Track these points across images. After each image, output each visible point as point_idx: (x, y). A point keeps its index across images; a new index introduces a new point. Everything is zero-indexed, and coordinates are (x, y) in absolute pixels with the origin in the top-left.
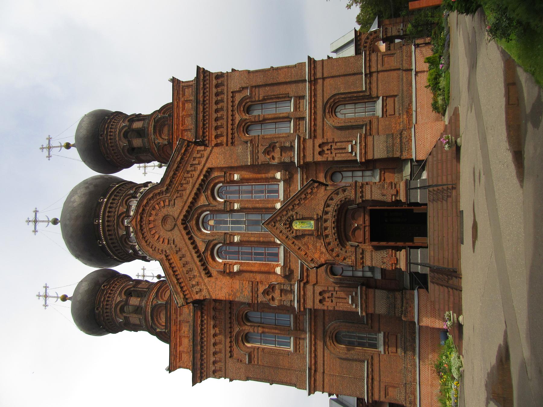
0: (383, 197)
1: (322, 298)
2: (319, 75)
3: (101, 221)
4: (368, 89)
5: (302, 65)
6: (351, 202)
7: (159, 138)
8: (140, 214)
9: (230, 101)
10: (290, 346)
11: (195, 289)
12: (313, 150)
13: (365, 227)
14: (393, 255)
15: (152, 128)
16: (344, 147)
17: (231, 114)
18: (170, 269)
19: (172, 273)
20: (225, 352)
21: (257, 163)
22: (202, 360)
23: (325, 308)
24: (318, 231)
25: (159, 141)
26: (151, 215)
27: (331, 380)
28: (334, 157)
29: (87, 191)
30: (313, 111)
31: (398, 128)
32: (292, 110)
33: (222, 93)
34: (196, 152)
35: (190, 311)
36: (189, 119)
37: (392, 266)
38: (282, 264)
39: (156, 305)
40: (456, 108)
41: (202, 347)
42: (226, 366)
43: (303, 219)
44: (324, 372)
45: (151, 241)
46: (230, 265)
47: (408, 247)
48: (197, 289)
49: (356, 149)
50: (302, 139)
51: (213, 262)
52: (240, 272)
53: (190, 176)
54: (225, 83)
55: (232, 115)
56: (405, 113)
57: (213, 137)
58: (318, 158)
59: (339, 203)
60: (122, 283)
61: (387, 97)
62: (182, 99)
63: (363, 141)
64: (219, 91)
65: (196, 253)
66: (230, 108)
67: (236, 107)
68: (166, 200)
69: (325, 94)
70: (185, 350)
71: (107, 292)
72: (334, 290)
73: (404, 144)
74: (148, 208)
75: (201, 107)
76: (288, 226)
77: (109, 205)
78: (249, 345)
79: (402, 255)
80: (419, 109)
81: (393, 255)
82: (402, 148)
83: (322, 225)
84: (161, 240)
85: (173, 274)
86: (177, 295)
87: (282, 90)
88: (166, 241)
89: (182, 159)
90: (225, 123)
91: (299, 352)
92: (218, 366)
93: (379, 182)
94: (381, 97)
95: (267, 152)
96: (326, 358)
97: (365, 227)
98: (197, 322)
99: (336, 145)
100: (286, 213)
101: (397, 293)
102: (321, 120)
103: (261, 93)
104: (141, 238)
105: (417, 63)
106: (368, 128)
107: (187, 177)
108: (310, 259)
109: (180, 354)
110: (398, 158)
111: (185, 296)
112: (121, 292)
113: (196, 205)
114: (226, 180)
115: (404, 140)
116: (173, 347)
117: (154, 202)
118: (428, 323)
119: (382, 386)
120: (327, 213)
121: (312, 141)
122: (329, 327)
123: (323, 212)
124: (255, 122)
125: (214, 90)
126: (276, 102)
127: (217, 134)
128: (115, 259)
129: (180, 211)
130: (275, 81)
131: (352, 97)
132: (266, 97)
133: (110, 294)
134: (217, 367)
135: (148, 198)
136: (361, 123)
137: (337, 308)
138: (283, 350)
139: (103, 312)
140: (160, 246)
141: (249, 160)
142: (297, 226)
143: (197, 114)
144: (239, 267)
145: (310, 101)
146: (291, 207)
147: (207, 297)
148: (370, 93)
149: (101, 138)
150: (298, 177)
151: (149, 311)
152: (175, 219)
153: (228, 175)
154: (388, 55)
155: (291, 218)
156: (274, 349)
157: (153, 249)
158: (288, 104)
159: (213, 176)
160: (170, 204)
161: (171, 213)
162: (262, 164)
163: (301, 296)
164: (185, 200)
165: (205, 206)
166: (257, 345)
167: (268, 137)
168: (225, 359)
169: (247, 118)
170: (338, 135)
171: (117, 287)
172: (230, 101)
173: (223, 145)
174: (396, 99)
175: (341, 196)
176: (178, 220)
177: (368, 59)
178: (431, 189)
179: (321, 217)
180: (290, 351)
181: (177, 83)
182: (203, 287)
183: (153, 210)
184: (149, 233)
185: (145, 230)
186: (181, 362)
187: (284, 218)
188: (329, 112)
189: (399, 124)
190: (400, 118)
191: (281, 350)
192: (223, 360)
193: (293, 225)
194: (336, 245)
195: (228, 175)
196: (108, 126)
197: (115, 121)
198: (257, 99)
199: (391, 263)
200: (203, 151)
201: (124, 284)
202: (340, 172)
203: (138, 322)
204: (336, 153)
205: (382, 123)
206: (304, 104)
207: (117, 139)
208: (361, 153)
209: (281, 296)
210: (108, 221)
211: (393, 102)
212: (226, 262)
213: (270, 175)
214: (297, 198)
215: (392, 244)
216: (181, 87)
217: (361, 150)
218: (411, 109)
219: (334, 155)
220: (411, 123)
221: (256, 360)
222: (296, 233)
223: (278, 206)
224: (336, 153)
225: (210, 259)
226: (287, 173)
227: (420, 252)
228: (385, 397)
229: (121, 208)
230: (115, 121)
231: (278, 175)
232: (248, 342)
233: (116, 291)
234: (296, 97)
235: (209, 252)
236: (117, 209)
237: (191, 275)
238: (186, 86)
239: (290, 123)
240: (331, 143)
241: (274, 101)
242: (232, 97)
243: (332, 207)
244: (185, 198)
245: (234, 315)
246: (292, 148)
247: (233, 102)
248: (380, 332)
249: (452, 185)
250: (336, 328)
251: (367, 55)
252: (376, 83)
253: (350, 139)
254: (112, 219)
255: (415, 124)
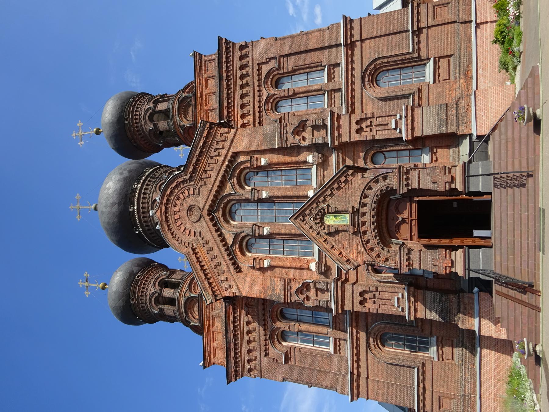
0: (434, 185)
1: (363, 299)
2: (356, 37)
3: (135, 208)
4: (415, 50)
5: (336, 26)
6: (393, 191)
7: (184, 119)
8: (164, 205)
9: (255, 75)
10: (329, 346)
11: (224, 284)
12: (350, 128)
13: (411, 221)
14: (448, 256)
15: (177, 110)
16: (386, 123)
17: (258, 89)
18: (197, 263)
19: (199, 268)
20: (260, 350)
21: (285, 146)
22: (236, 358)
23: (367, 311)
24: (354, 227)
25: (185, 123)
26: (176, 205)
27: (376, 387)
28: (374, 136)
29: (122, 177)
30: (350, 81)
31: (453, 95)
32: (326, 81)
33: (247, 66)
34: (220, 134)
35: (222, 306)
36: (213, 97)
37: (446, 269)
38: (317, 260)
39: (188, 298)
40: (533, 67)
41: (235, 345)
42: (261, 365)
43: (337, 213)
44: (368, 378)
45: (177, 234)
46: (260, 260)
47: (467, 246)
48: (226, 284)
49: (401, 125)
50: (336, 116)
51: (242, 256)
52: (271, 268)
53: (214, 162)
54: (250, 55)
55: (259, 91)
56: (462, 77)
57: (239, 116)
58: (356, 137)
59: (379, 193)
60: (156, 274)
61: (440, 58)
62: (205, 76)
63: (409, 114)
64: (243, 64)
65: (224, 246)
66: (256, 83)
67: (263, 81)
68: (191, 189)
69: (364, 59)
70: (219, 346)
71: (141, 283)
72: (377, 291)
73: (461, 115)
74: (172, 198)
75: (225, 84)
76: (318, 221)
77: (143, 191)
78: (284, 344)
79: (458, 255)
80: (481, 70)
81: (448, 256)
82: (459, 121)
83: (358, 220)
84: (187, 232)
85: (200, 269)
86: (205, 292)
87: (314, 57)
88: (192, 233)
89: (205, 143)
90: (251, 101)
91: (340, 353)
92: (253, 364)
93: (430, 163)
94: (432, 59)
95: (297, 131)
96: (369, 361)
97: (411, 221)
98: (229, 319)
99: (376, 120)
100: (316, 205)
101: (452, 296)
102: (360, 91)
103: (290, 63)
104: (166, 230)
105: (478, 12)
106: (416, 97)
107: (211, 163)
108: (346, 260)
109: (214, 351)
110: (454, 133)
111: (214, 292)
112: (154, 283)
113: (222, 193)
114: (253, 165)
115: (461, 111)
116: (207, 343)
117: (179, 191)
118: (492, 332)
119: (436, 397)
120: (364, 205)
121: (347, 117)
122: (373, 328)
123: (360, 205)
124: (284, 97)
125: (238, 63)
126: (307, 73)
127: (243, 114)
128: (153, 246)
129: (205, 200)
130: (305, 48)
131: (397, 61)
132: (295, 68)
133: (144, 284)
134: (252, 366)
135: (172, 187)
136: (408, 92)
137: (379, 311)
138: (322, 351)
139: (138, 302)
140: (186, 238)
141: (277, 142)
142: (330, 220)
143: (220, 91)
144: (270, 262)
145: (346, 69)
146: (321, 199)
147: (237, 294)
148: (419, 54)
149: (126, 122)
150: (333, 158)
151: (183, 303)
152: (200, 209)
153: (255, 159)
154: (440, 5)
155: (322, 211)
156: (312, 349)
157: (180, 242)
158: (321, 74)
159: (239, 161)
160: (195, 193)
161: (196, 203)
162: (291, 147)
163: (339, 296)
164: (210, 189)
165: (230, 195)
166: (294, 344)
167: (300, 113)
168: (260, 357)
169: (276, 93)
170: (379, 108)
171: (151, 277)
172: (255, 75)
173: (250, 125)
174: (451, 59)
175: (381, 184)
176: (204, 211)
177: (416, 12)
178: (496, 176)
179: (358, 210)
180: (329, 352)
181: (199, 58)
182: (232, 283)
183: (178, 199)
184: (174, 225)
185: (170, 221)
186: (215, 358)
187: (315, 212)
188: (369, 81)
189: (455, 90)
190: (456, 83)
191: (319, 350)
192: (258, 359)
193: (325, 218)
194: (376, 244)
195: (255, 159)
196: (133, 109)
197: (140, 103)
198: (286, 71)
199: (444, 266)
200: (226, 133)
201: (158, 275)
202: (382, 152)
203: (172, 314)
204: (376, 131)
205: (433, 90)
206: (339, 73)
207: (143, 123)
208: (407, 130)
209: (317, 295)
210: (143, 208)
211: (448, 64)
212: (256, 257)
213: (301, 158)
214: (328, 187)
215: (445, 242)
216: (203, 62)
217: (407, 125)
218: (470, 71)
219: (374, 132)
220: (470, 88)
221: (293, 360)
222: (328, 229)
223: (311, 193)
224: (376, 131)
225: (239, 253)
226: (320, 155)
227: (482, 253)
228: (439, 408)
229: (154, 193)
230: (140, 103)
231: (310, 158)
232: (286, 341)
233: (150, 282)
234: (330, 65)
235: (237, 246)
236: (151, 195)
237: (220, 269)
238: (208, 61)
239: (324, 95)
240: (371, 118)
241: (305, 71)
242: (258, 70)
243: (370, 198)
244: (210, 186)
245: (268, 312)
246: (324, 126)
247: (259, 75)
248: (431, 335)
249: (528, 172)
250: (381, 330)
251: (415, 8)
252: (425, 42)
253: (394, 113)
254: (146, 205)
255: (475, 90)
